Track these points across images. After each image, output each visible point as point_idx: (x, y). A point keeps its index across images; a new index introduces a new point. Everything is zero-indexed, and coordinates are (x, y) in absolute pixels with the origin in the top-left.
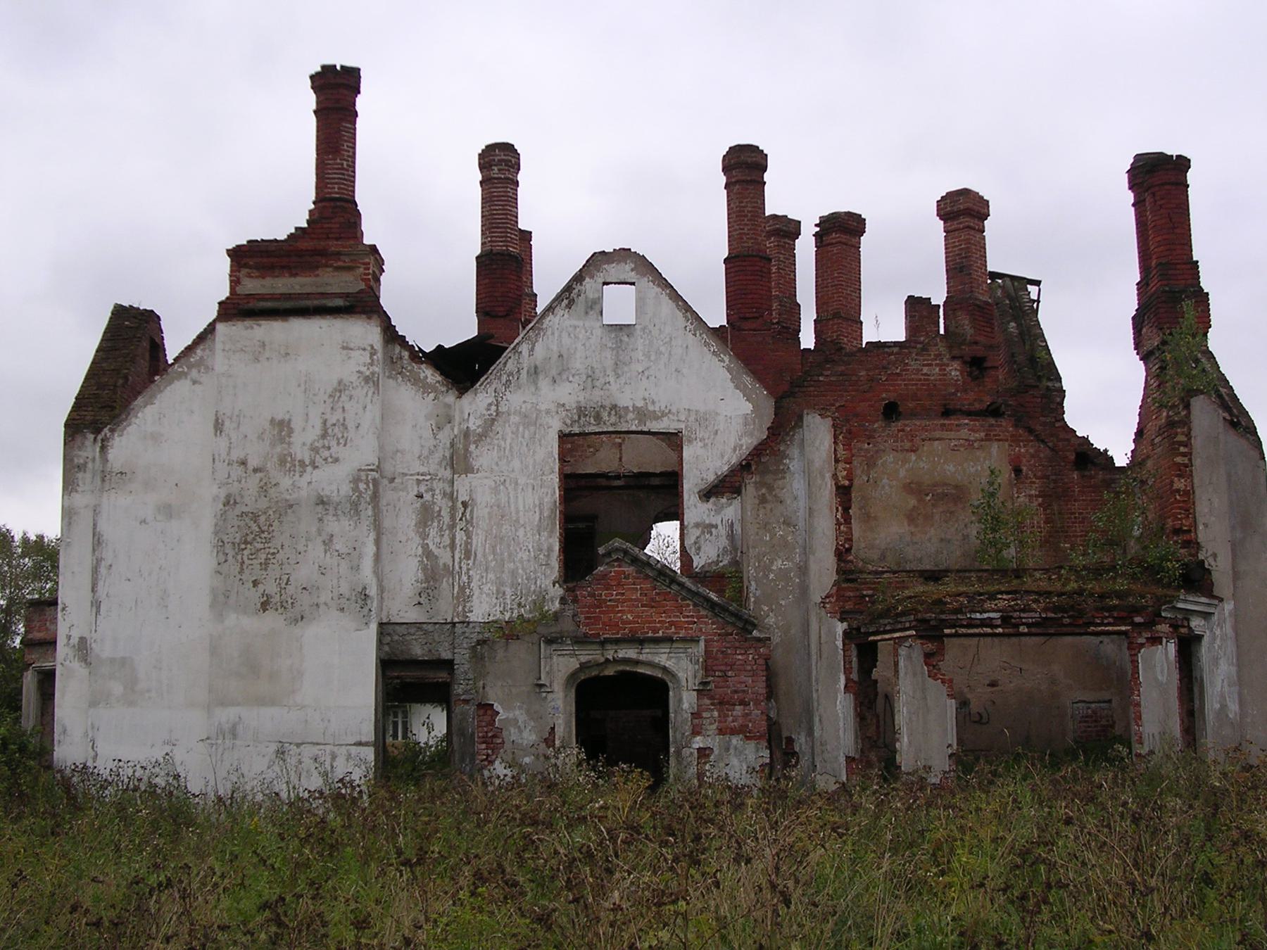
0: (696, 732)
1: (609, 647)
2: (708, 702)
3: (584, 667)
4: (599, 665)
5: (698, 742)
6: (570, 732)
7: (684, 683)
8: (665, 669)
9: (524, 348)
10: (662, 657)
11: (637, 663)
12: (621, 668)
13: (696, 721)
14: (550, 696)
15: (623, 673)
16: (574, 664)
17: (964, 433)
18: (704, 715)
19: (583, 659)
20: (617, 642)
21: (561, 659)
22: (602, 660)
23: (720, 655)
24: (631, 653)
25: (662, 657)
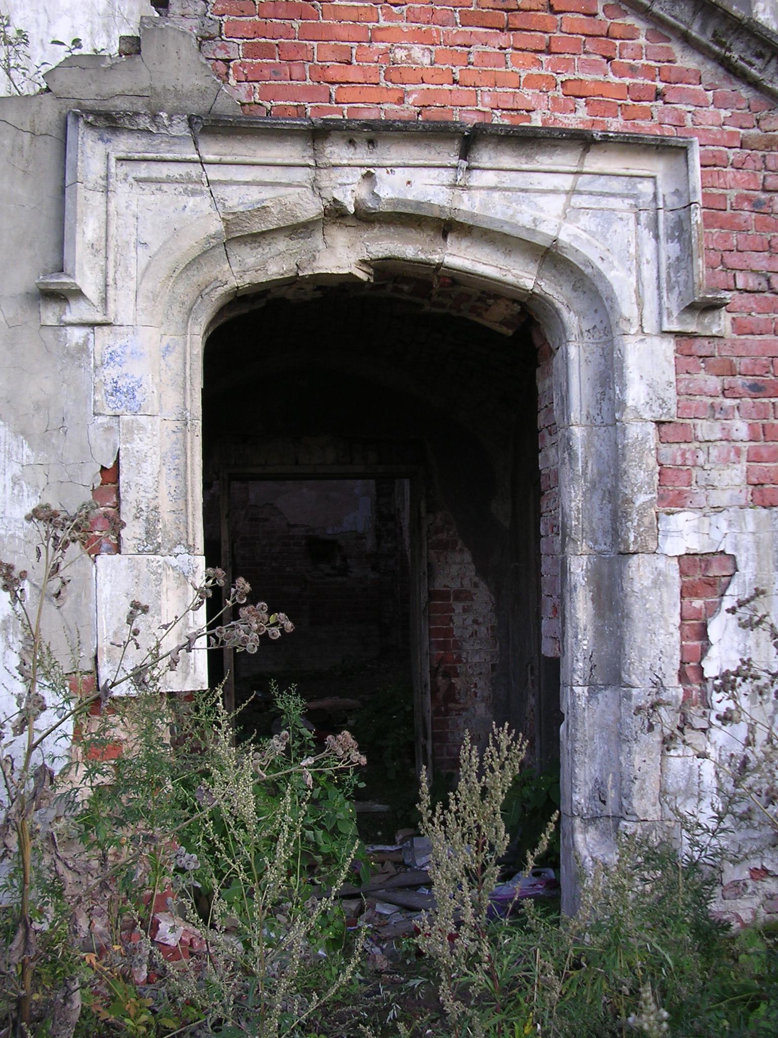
0: (673, 498)
1: (337, 152)
2: (714, 383)
3: (239, 234)
4: (298, 229)
5: (684, 533)
6: (184, 495)
7: (627, 307)
8: (550, 256)
9: (688, 58)
10: (534, 197)
11: (447, 227)
12: (408, 248)
13: (672, 452)
14: (102, 340)
15: (384, 269)
16: (201, 218)
17: (598, 514)
18: (705, 429)
19: (239, 199)
20: (374, 133)
21: (148, 197)
22: (311, 208)
23: (747, 215)
24: (416, 179)
25: (534, 197)
